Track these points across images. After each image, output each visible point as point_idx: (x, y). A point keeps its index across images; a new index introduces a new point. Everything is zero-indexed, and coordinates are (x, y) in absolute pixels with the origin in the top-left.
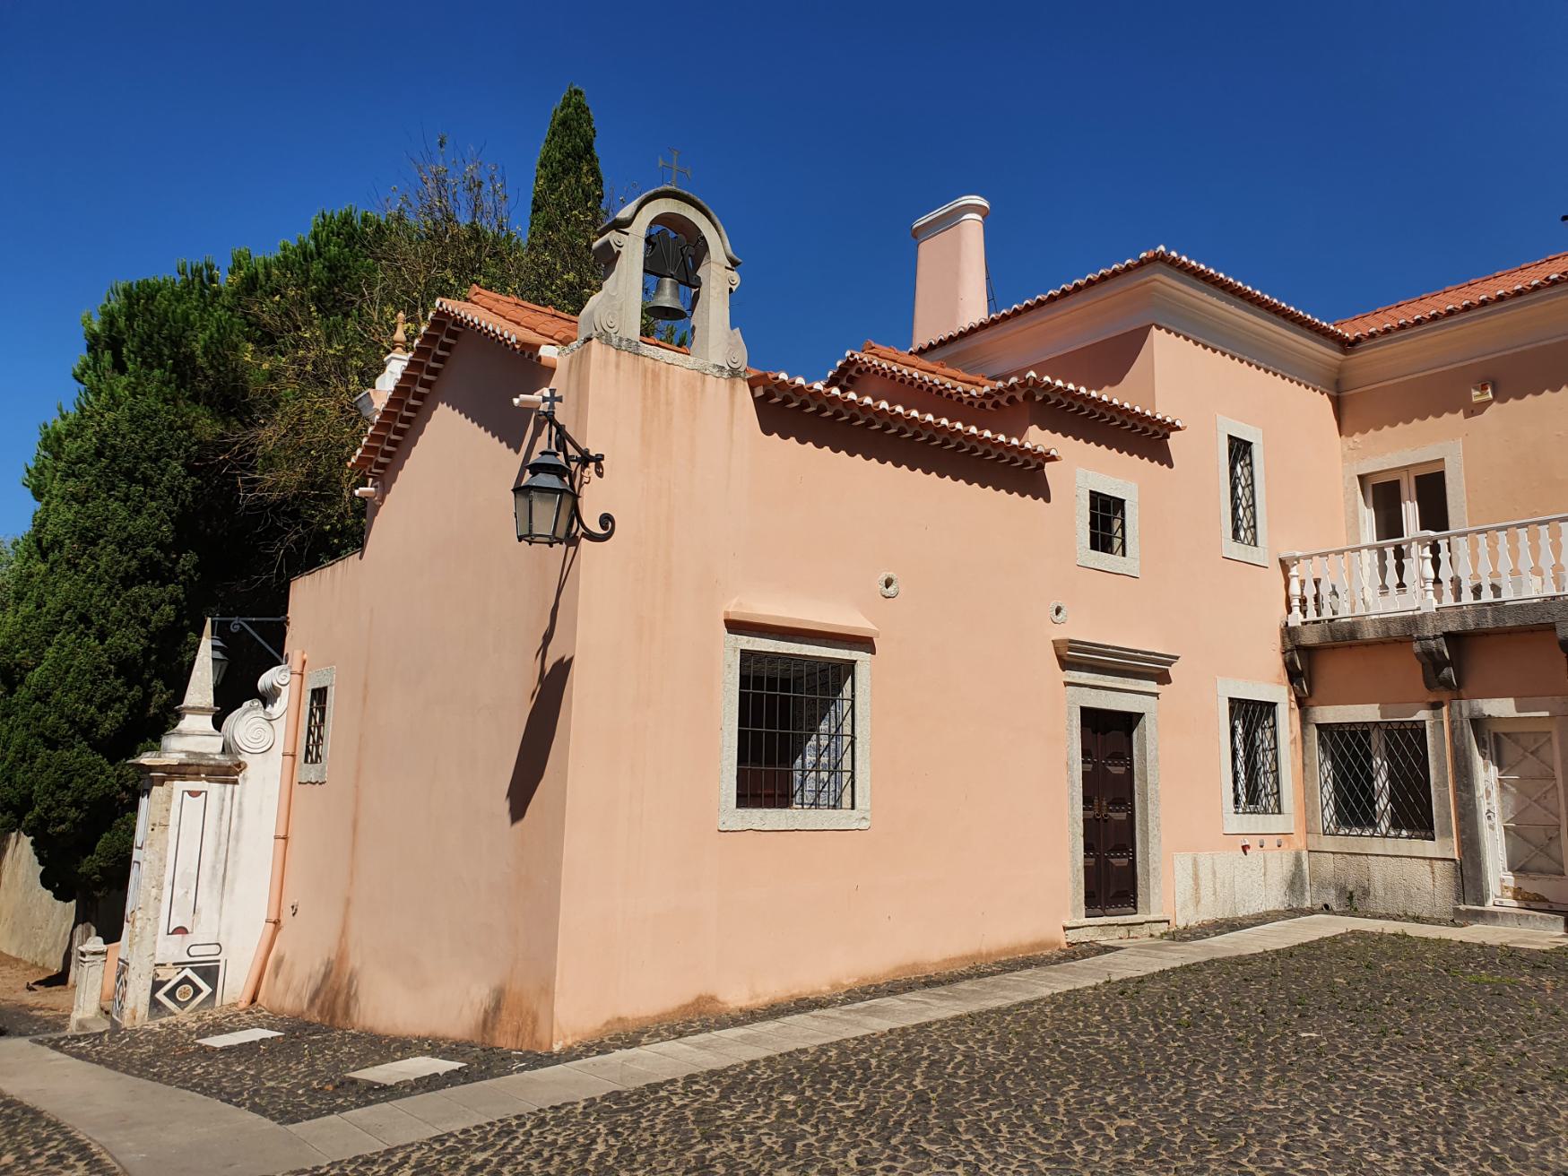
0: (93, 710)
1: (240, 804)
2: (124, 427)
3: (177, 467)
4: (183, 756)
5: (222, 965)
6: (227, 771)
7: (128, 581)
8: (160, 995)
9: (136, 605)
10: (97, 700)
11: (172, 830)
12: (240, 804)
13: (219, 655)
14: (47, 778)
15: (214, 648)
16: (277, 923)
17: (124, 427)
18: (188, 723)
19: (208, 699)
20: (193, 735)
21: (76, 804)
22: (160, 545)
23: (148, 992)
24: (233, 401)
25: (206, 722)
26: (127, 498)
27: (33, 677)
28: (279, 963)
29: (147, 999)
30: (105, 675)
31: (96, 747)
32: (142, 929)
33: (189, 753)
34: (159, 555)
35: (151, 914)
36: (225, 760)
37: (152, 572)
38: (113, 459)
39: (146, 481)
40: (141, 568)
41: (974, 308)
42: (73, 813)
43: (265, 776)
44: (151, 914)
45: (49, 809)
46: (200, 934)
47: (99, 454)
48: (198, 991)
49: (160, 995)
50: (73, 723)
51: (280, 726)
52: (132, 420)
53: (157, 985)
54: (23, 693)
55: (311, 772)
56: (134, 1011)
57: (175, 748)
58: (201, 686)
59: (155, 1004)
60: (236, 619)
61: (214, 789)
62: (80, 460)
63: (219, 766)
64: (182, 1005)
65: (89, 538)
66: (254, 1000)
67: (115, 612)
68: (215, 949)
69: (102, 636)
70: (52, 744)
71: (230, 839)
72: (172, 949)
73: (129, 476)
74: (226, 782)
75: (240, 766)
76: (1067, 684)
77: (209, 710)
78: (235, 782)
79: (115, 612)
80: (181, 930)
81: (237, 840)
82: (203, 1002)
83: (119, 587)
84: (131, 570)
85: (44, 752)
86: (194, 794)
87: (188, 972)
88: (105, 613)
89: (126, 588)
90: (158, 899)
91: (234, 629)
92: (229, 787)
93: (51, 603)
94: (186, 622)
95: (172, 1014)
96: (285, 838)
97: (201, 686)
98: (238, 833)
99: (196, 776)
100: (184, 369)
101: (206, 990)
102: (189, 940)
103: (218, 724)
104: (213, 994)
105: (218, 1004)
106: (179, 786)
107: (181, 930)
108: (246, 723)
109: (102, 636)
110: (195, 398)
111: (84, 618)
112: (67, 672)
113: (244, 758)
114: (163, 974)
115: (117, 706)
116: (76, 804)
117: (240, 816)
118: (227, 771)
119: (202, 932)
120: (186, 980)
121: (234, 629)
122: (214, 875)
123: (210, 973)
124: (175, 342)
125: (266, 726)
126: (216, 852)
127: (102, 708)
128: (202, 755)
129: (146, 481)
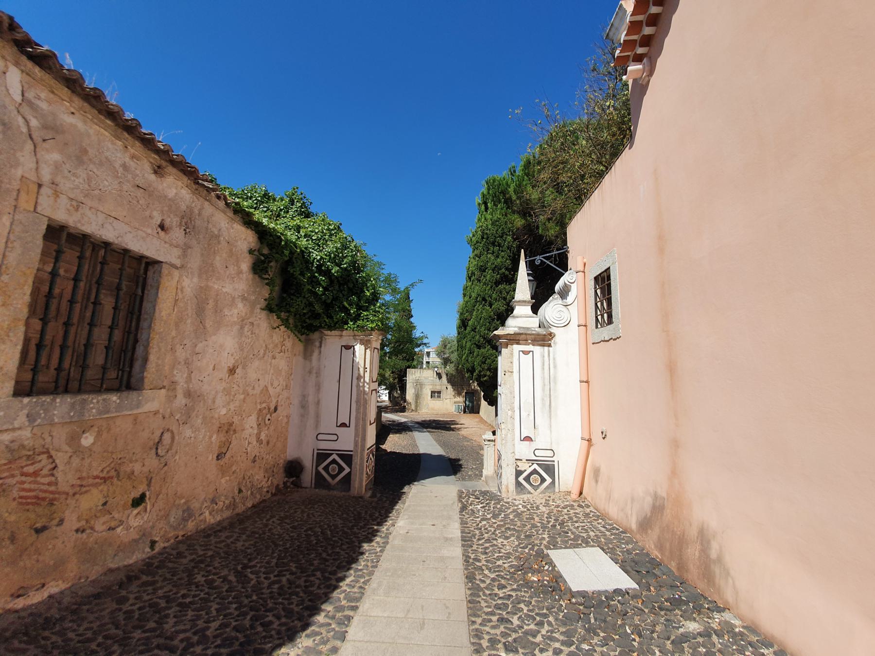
1: (554, 359)
2: (490, 227)
3: (509, 238)
4: (516, 329)
5: (556, 464)
6: (544, 339)
7: (497, 283)
8: (521, 479)
9: (501, 292)
11: (516, 375)
12: (554, 359)
13: (531, 278)
14: (479, 359)
15: (528, 275)
16: (589, 440)
17: (490, 227)
18: (519, 310)
19: (528, 297)
20: (522, 318)
22: (507, 269)
23: (514, 477)
24: (526, 212)
25: (528, 310)
26: (493, 253)
27: (470, 323)
28: (597, 472)
29: (514, 481)
30: (493, 320)
32: (506, 435)
33: (520, 328)
34: (507, 273)
35: (509, 426)
36: (542, 331)
38: (487, 238)
39: (499, 245)
40: (501, 278)
42: (488, 373)
43: (568, 343)
44: (509, 426)
45: (480, 372)
46: (540, 443)
47: (483, 238)
48: (543, 480)
49: (521, 479)
50: (484, 338)
51: (573, 309)
52: (492, 224)
53: (519, 473)
54: (468, 329)
55: (606, 332)
56: (507, 487)
57: (512, 325)
58: (523, 287)
59: (518, 484)
60: (538, 257)
61: (537, 350)
62: (477, 242)
63: (538, 335)
64: (536, 488)
65: (482, 269)
66: (581, 493)
68: (550, 453)
69: (491, 305)
70: (479, 347)
71: (551, 382)
72: (525, 451)
73: (493, 244)
74: (544, 346)
75: (551, 335)
77: (529, 302)
78: (550, 346)
79: (494, 296)
80: (528, 439)
81: (555, 383)
82: (547, 488)
85: (476, 350)
86: (526, 353)
87: (535, 466)
88: (490, 296)
90: (512, 418)
91: (538, 263)
92: (546, 348)
93: (474, 295)
95: (530, 493)
96: (587, 382)
97: (523, 287)
98: (555, 378)
99: (526, 342)
100: (508, 202)
101: (549, 480)
102: (534, 445)
103: (535, 309)
104: (553, 482)
105: (557, 490)
106: (516, 348)
107: (528, 439)
108: (551, 309)
109: (491, 305)
110: (514, 212)
111: (484, 299)
113: (553, 330)
114: (523, 466)
117: (555, 367)
118: (544, 339)
119: (540, 443)
120: (535, 472)
121: (538, 263)
122: (543, 404)
123: (550, 469)
124: (504, 193)
125: (564, 309)
126: (543, 390)
128: (528, 328)
129: (499, 245)
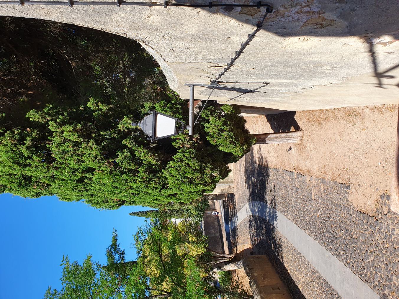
0: (141, 170)
7: (49, 159)
9: (64, 152)
10: (133, 167)
21: (202, 171)
30: (116, 165)
31: (164, 164)
37: (41, 146)
41: (248, 245)
42: (208, 171)
67: (73, 164)
76: (133, 214)
79: (73, 164)
83: (55, 164)
84: (40, 159)
88: (74, 171)
89: (54, 160)
94: (82, 108)
112: (117, 188)
115: (136, 153)
116: (202, 171)
127: (139, 163)
